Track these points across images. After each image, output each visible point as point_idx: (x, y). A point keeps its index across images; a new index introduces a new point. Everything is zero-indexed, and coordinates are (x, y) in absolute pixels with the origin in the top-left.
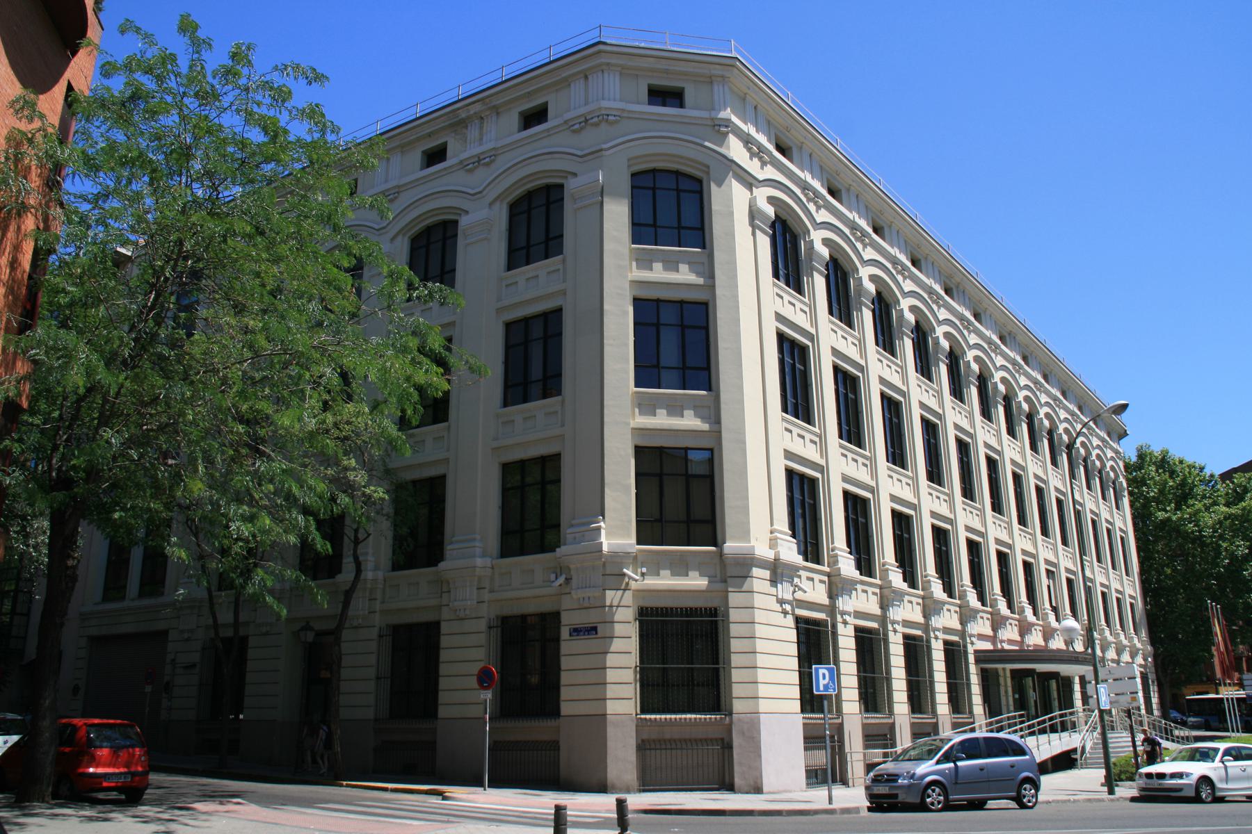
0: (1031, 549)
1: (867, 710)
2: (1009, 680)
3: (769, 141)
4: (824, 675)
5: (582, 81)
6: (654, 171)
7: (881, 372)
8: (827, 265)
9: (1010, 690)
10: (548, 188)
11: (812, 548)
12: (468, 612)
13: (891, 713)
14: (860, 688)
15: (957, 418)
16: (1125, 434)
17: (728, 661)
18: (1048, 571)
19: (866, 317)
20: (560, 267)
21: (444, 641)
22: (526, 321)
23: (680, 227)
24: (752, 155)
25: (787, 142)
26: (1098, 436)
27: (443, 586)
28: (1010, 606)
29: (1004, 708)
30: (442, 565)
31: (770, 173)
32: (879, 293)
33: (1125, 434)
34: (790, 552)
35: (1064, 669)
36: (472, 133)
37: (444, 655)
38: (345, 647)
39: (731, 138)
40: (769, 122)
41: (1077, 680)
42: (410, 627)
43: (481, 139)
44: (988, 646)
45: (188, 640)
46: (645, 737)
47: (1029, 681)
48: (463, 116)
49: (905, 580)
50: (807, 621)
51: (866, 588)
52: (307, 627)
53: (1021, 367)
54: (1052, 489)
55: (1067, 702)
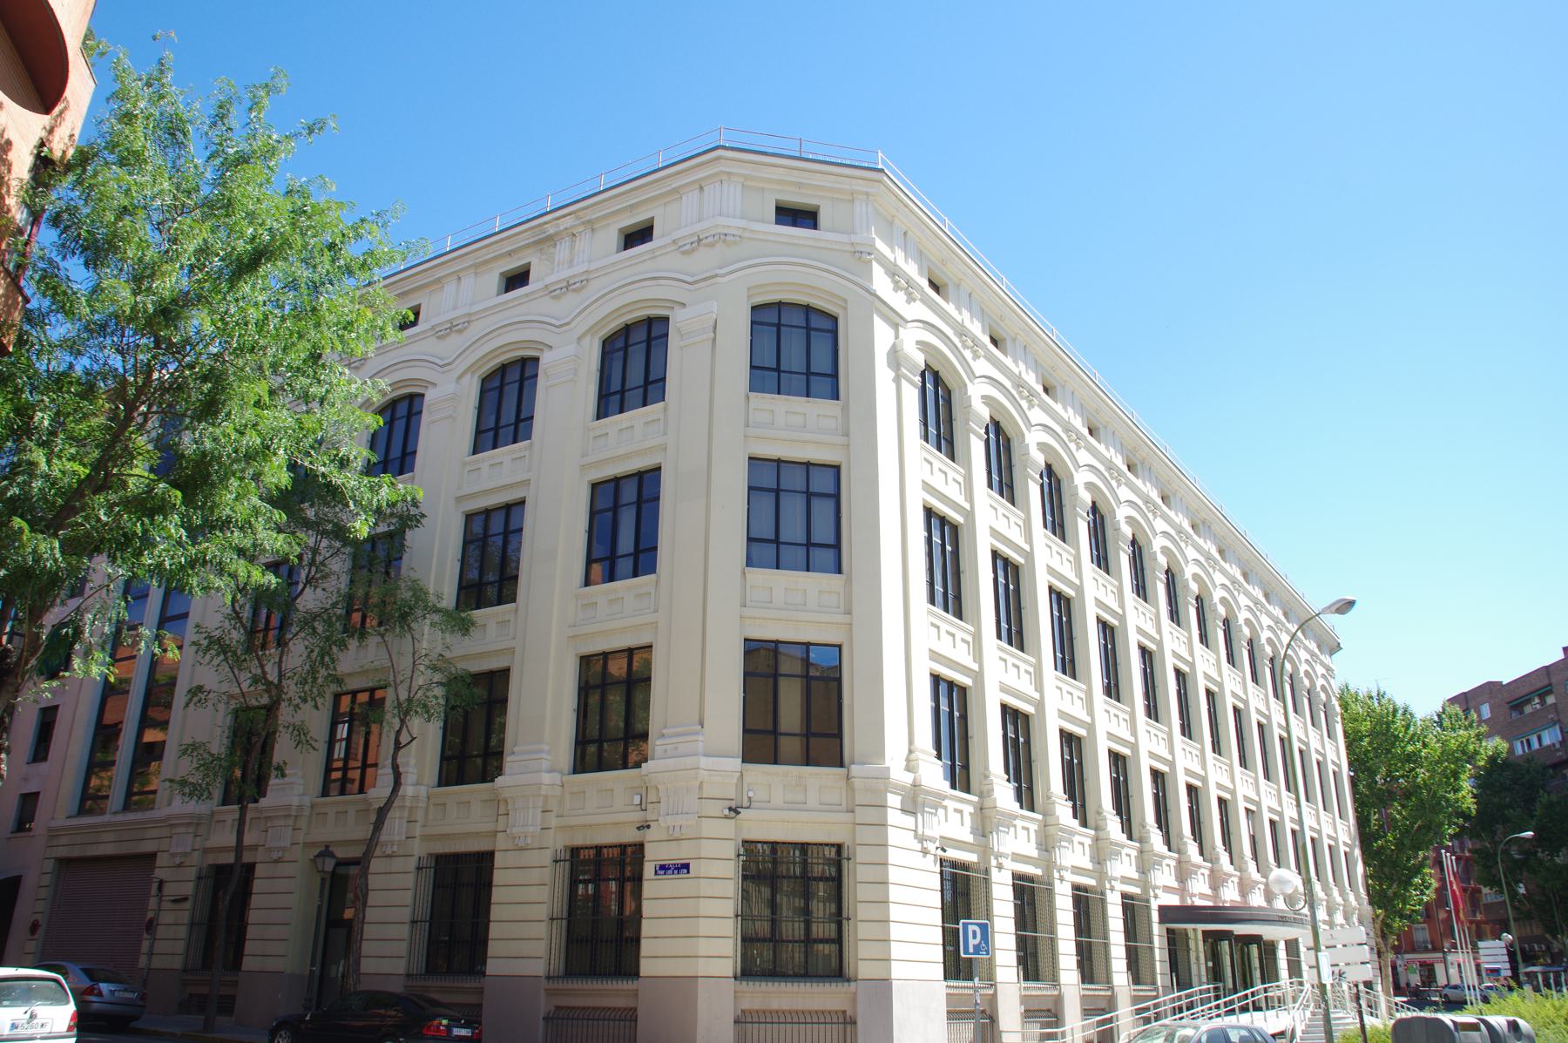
0: (1198, 770)
1: (1026, 979)
2: (1201, 943)
3: (921, 274)
4: (974, 933)
5: (696, 192)
6: (779, 305)
7: (1098, 594)
9: (1202, 956)
10: (650, 322)
11: (961, 775)
12: (529, 840)
14: (1018, 950)
15: (1141, 621)
16: (1339, 647)
18: (1247, 810)
19: (1082, 529)
20: (661, 416)
21: (499, 877)
22: (617, 481)
23: (809, 373)
24: (897, 288)
25: (1052, 382)
26: (1306, 649)
27: (498, 805)
28: (1168, 842)
29: (1195, 980)
30: (500, 780)
31: (917, 310)
32: (1049, 467)
33: (1339, 647)
34: (933, 774)
35: (1267, 932)
36: (562, 251)
37: (497, 895)
38: (374, 881)
41: (1282, 946)
42: (457, 858)
43: (571, 261)
44: (1173, 900)
45: (180, 865)
46: (746, 1005)
47: (1225, 945)
48: (552, 231)
49: (1075, 817)
50: (954, 864)
51: (1026, 824)
52: (326, 852)
53: (1263, 606)
54: (1253, 710)
55: (1269, 974)
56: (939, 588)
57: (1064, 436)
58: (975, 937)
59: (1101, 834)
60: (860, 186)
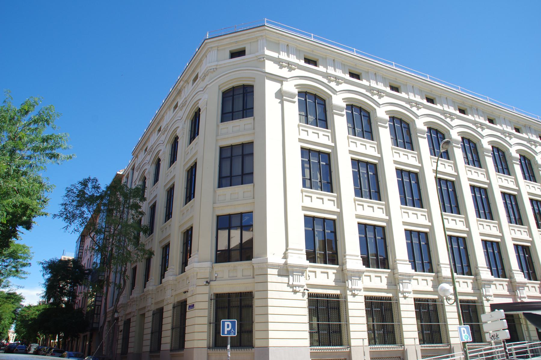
4: (228, 325)
8: (520, 159)
13: (402, 344)
17: (347, 321)
24: (281, 67)
39: (267, 61)
40: (510, 121)
56: (512, 217)
57: (369, 94)
58: (228, 327)
59: (439, 274)
60: (258, 34)
